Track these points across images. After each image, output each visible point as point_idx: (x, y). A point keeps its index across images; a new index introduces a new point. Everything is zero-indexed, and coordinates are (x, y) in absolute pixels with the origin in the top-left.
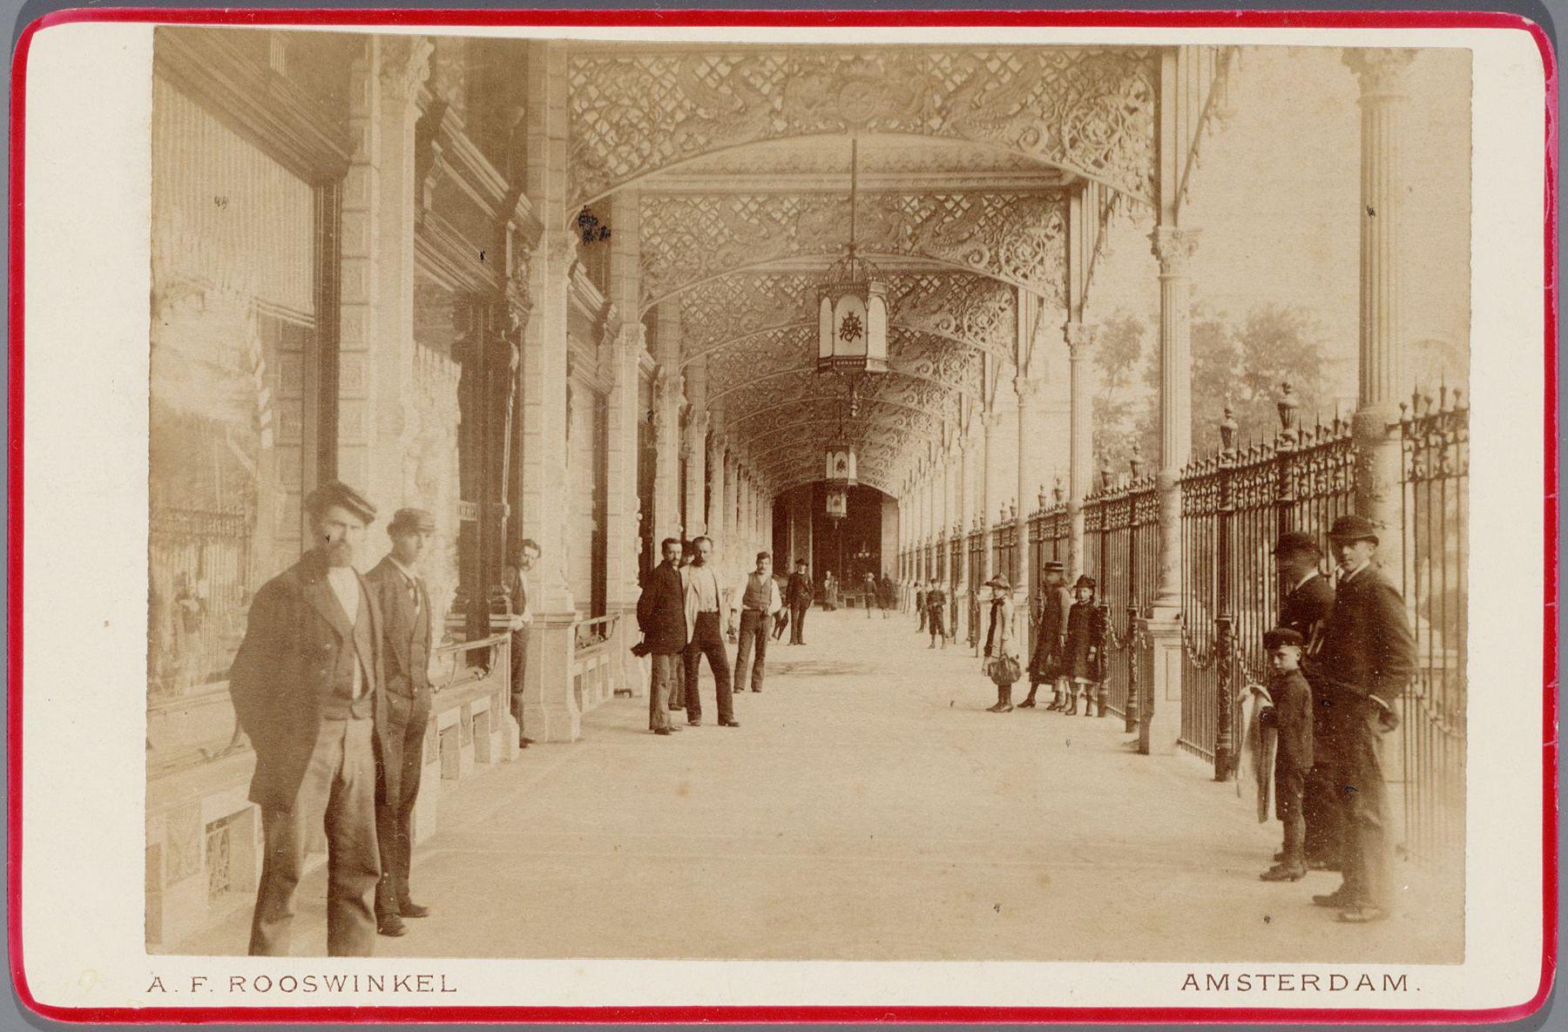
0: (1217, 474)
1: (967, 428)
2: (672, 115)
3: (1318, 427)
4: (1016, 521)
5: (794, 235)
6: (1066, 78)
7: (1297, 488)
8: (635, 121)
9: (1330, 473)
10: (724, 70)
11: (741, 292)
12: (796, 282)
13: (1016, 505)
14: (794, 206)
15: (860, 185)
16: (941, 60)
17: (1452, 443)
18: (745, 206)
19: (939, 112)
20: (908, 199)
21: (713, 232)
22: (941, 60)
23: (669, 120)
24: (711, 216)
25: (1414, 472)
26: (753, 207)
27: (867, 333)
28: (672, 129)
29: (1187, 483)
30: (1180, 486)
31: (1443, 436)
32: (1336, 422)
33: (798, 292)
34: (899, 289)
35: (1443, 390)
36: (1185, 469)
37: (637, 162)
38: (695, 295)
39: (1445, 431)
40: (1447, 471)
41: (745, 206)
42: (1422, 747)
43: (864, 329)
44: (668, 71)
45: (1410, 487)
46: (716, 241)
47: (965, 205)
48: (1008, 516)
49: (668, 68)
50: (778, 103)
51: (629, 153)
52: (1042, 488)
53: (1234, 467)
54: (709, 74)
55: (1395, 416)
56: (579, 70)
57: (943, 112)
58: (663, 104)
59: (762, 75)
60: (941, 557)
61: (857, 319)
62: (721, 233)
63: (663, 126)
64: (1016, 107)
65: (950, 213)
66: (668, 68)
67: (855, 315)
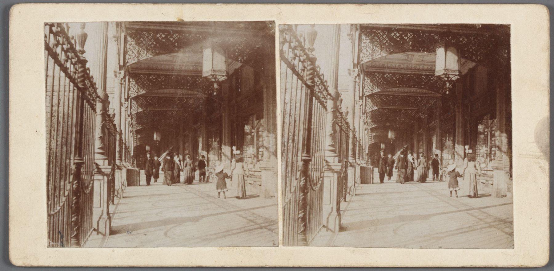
11: (151, 39)
12: (409, 35)
58: (383, 41)
59: (407, 37)
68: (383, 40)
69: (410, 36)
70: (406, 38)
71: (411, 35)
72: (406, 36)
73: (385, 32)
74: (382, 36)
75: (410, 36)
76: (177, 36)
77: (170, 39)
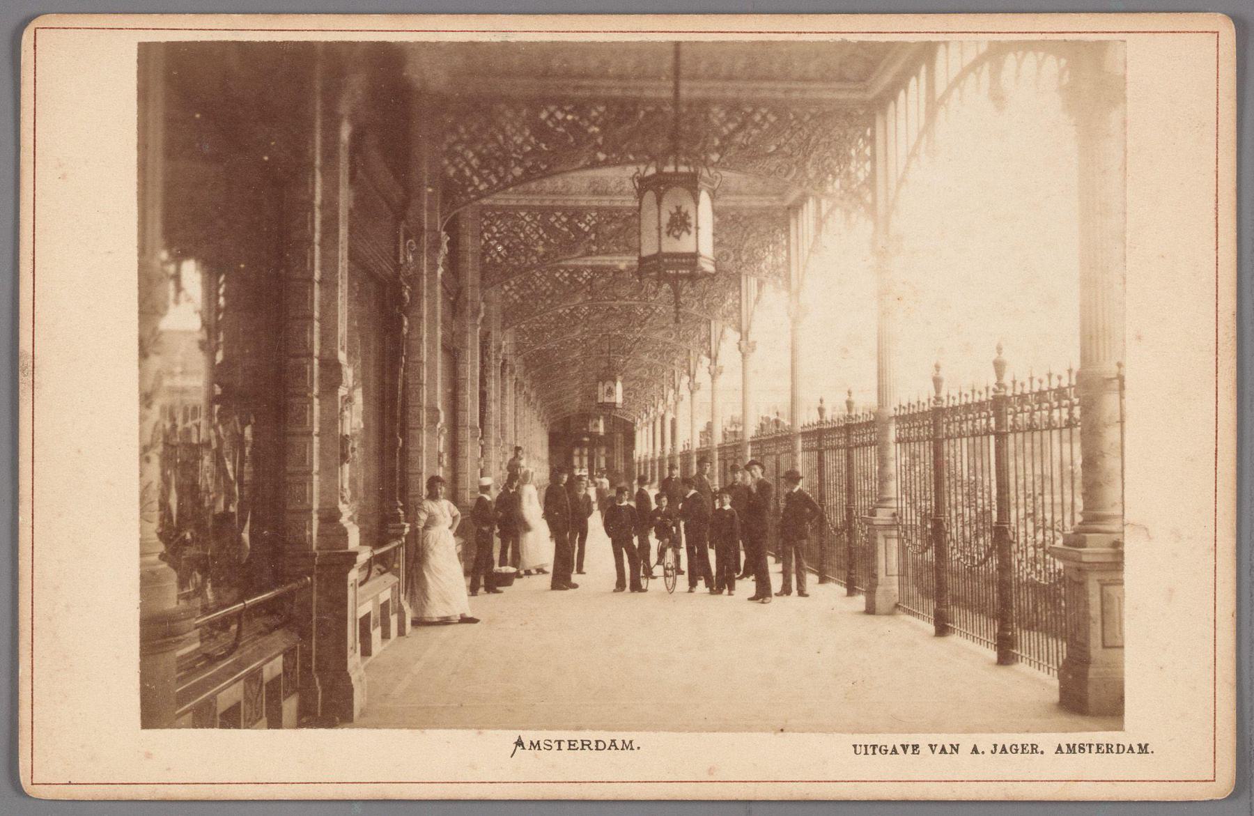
0: (844, 427)
1: (694, 375)
3: (900, 406)
4: (711, 447)
5: (601, 144)
7: (945, 431)
8: (493, 150)
9: (970, 422)
10: (567, 311)
13: (690, 442)
14: (594, 218)
15: (684, 93)
17: (1056, 408)
18: (562, 274)
19: (654, 292)
21: (519, 140)
23: (519, 151)
24: (533, 225)
25: (973, 431)
26: (564, 219)
27: (697, 228)
28: (521, 157)
29: (753, 443)
30: (894, 421)
31: (974, 414)
32: (909, 404)
33: (591, 227)
35: (1014, 382)
36: (898, 407)
37: (495, 182)
38: (495, 230)
39: (1016, 406)
40: (1035, 427)
41: (562, 274)
42: (1027, 645)
43: (694, 226)
44: (535, 219)
45: (898, 445)
46: (521, 149)
47: (772, 119)
48: (686, 448)
49: (535, 218)
50: (588, 288)
52: (849, 393)
53: (906, 413)
54: (556, 221)
55: (892, 413)
56: (487, 218)
57: (721, 150)
58: (515, 138)
60: (653, 468)
61: (686, 214)
62: (526, 141)
63: (514, 155)
64: (773, 148)
65: (757, 125)
66: (535, 218)
67: (683, 210)
68: (532, 233)
70: (583, 225)
74: (538, 278)
77: (579, 224)
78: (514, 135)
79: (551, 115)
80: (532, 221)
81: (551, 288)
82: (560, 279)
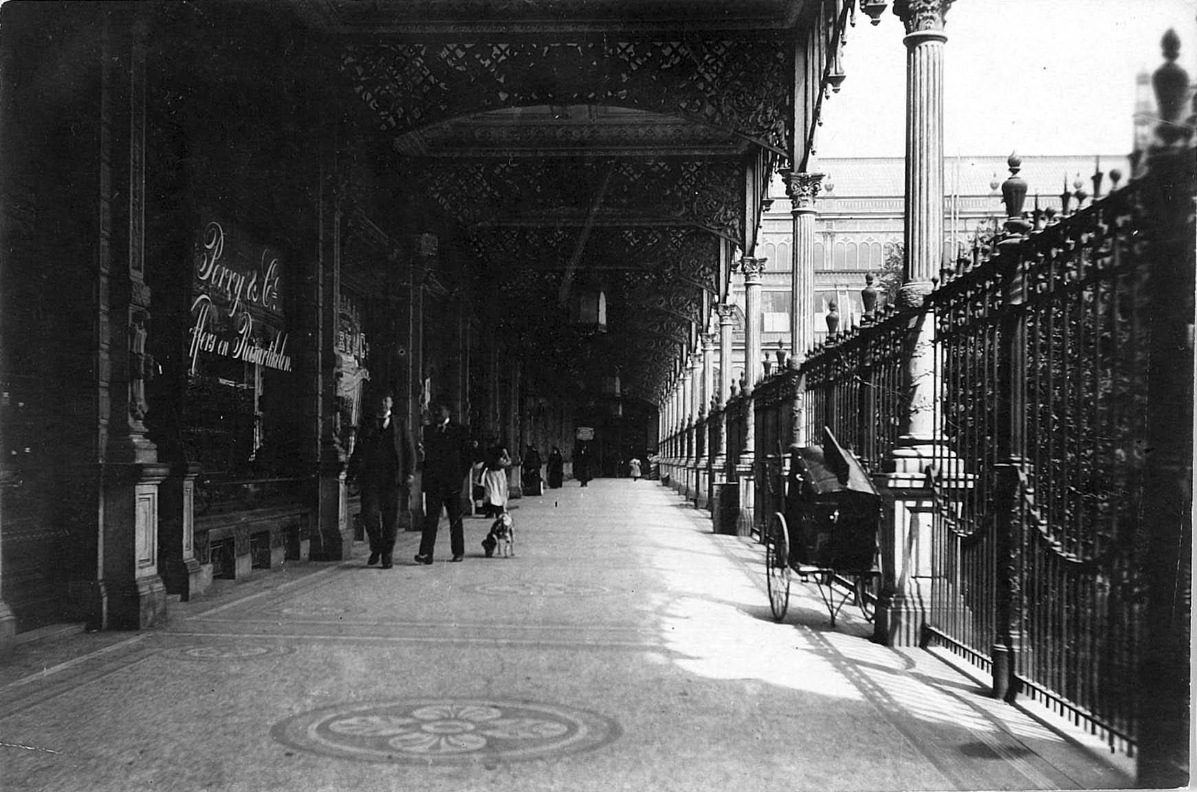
2: (480, 194)
6: (722, 61)
16: (628, 47)
20: (623, 45)
22: (628, 47)
34: (633, 60)
36: (938, 276)
51: (388, 116)
59: (491, 58)
69: (498, 56)
70: (488, 62)
71: (503, 52)
72: (487, 54)
73: (480, 168)
75: (498, 56)
76: (503, 52)
78: (413, 75)
79: (453, 53)
80: (476, 173)
81: (489, 189)
82: (449, 62)
